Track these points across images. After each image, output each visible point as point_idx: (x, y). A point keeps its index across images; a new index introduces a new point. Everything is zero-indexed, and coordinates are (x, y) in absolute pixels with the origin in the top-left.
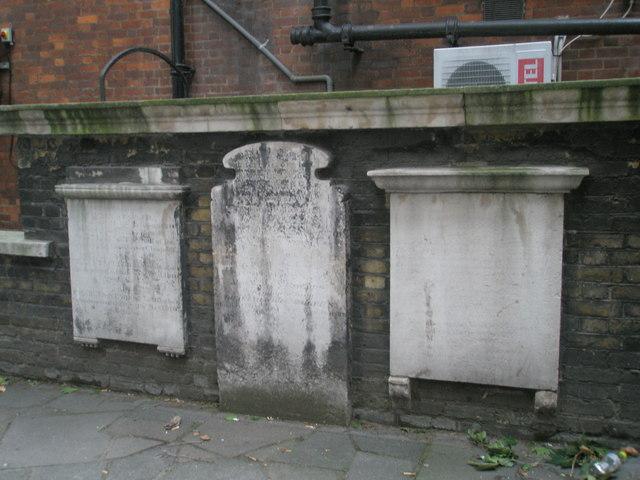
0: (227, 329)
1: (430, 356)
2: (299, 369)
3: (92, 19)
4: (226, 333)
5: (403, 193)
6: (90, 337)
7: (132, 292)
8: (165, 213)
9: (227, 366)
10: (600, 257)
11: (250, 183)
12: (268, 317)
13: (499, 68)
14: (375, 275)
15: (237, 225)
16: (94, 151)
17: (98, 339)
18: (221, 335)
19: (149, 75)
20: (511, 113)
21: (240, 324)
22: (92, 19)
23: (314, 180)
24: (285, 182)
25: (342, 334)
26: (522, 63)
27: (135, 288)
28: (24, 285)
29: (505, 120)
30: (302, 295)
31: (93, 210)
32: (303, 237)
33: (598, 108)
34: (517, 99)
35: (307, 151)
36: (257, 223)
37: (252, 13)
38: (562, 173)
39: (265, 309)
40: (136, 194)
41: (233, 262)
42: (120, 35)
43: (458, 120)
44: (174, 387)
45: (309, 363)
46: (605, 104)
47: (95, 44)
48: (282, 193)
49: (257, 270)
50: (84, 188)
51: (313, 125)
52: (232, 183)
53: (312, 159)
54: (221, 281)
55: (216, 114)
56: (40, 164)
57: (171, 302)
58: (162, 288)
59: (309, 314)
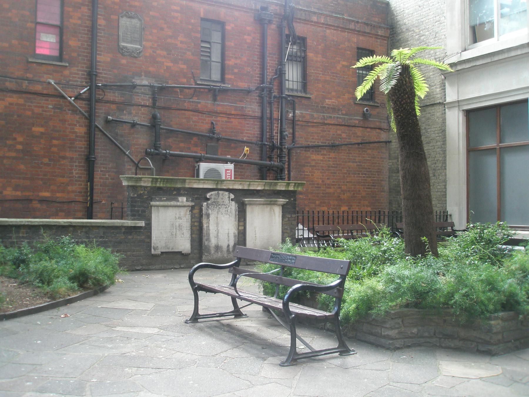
0: (206, 243)
1: (255, 245)
2: (225, 252)
3: (42, 130)
4: (206, 244)
5: (250, 204)
6: (158, 252)
7: (174, 236)
8: (187, 210)
9: (206, 254)
10: (287, 219)
11: (214, 202)
12: (218, 238)
13: (220, 171)
14: (242, 226)
15: (210, 213)
16: (161, 192)
17: (161, 252)
18: (204, 245)
19: (72, 158)
20: (273, 187)
21: (210, 241)
22: (42, 130)
23: (231, 201)
24: (223, 202)
25: (237, 241)
26: (226, 170)
27: (175, 234)
28: (130, 237)
29: (272, 188)
30: (227, 231)
31: (161, 210)
32: (228, 216)
33: (288, 187)
34: (275, 184)
35: (229, 194)
36: (216, 212)
37: (122, 139)
38: (282, 201)
39: (217, 236)
40: (179, 205)
41: (209, 224)
42: (57, 139)
43: (263, 188)
44: (184, 265)
45: (228, 250)
46: (290, 186)
47: (42, 141)
48: (223, 205)
49: (215, 225)
50: (158, 203)
51: (231, 187)
52: (209, 202)
53: (230, 196)
54: (205, 229)
55: (207, 183)
56: (140, 196)
57: (187, 237)
58: (184, 233)
59: (228, 237)
